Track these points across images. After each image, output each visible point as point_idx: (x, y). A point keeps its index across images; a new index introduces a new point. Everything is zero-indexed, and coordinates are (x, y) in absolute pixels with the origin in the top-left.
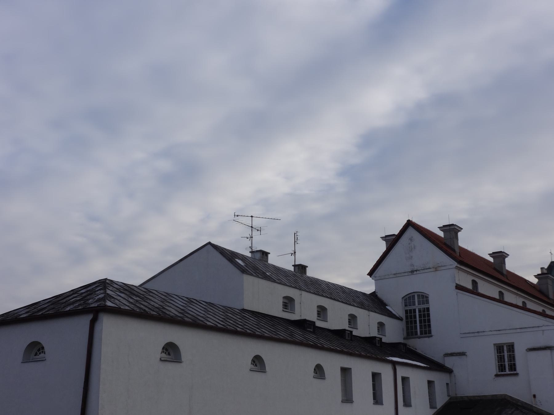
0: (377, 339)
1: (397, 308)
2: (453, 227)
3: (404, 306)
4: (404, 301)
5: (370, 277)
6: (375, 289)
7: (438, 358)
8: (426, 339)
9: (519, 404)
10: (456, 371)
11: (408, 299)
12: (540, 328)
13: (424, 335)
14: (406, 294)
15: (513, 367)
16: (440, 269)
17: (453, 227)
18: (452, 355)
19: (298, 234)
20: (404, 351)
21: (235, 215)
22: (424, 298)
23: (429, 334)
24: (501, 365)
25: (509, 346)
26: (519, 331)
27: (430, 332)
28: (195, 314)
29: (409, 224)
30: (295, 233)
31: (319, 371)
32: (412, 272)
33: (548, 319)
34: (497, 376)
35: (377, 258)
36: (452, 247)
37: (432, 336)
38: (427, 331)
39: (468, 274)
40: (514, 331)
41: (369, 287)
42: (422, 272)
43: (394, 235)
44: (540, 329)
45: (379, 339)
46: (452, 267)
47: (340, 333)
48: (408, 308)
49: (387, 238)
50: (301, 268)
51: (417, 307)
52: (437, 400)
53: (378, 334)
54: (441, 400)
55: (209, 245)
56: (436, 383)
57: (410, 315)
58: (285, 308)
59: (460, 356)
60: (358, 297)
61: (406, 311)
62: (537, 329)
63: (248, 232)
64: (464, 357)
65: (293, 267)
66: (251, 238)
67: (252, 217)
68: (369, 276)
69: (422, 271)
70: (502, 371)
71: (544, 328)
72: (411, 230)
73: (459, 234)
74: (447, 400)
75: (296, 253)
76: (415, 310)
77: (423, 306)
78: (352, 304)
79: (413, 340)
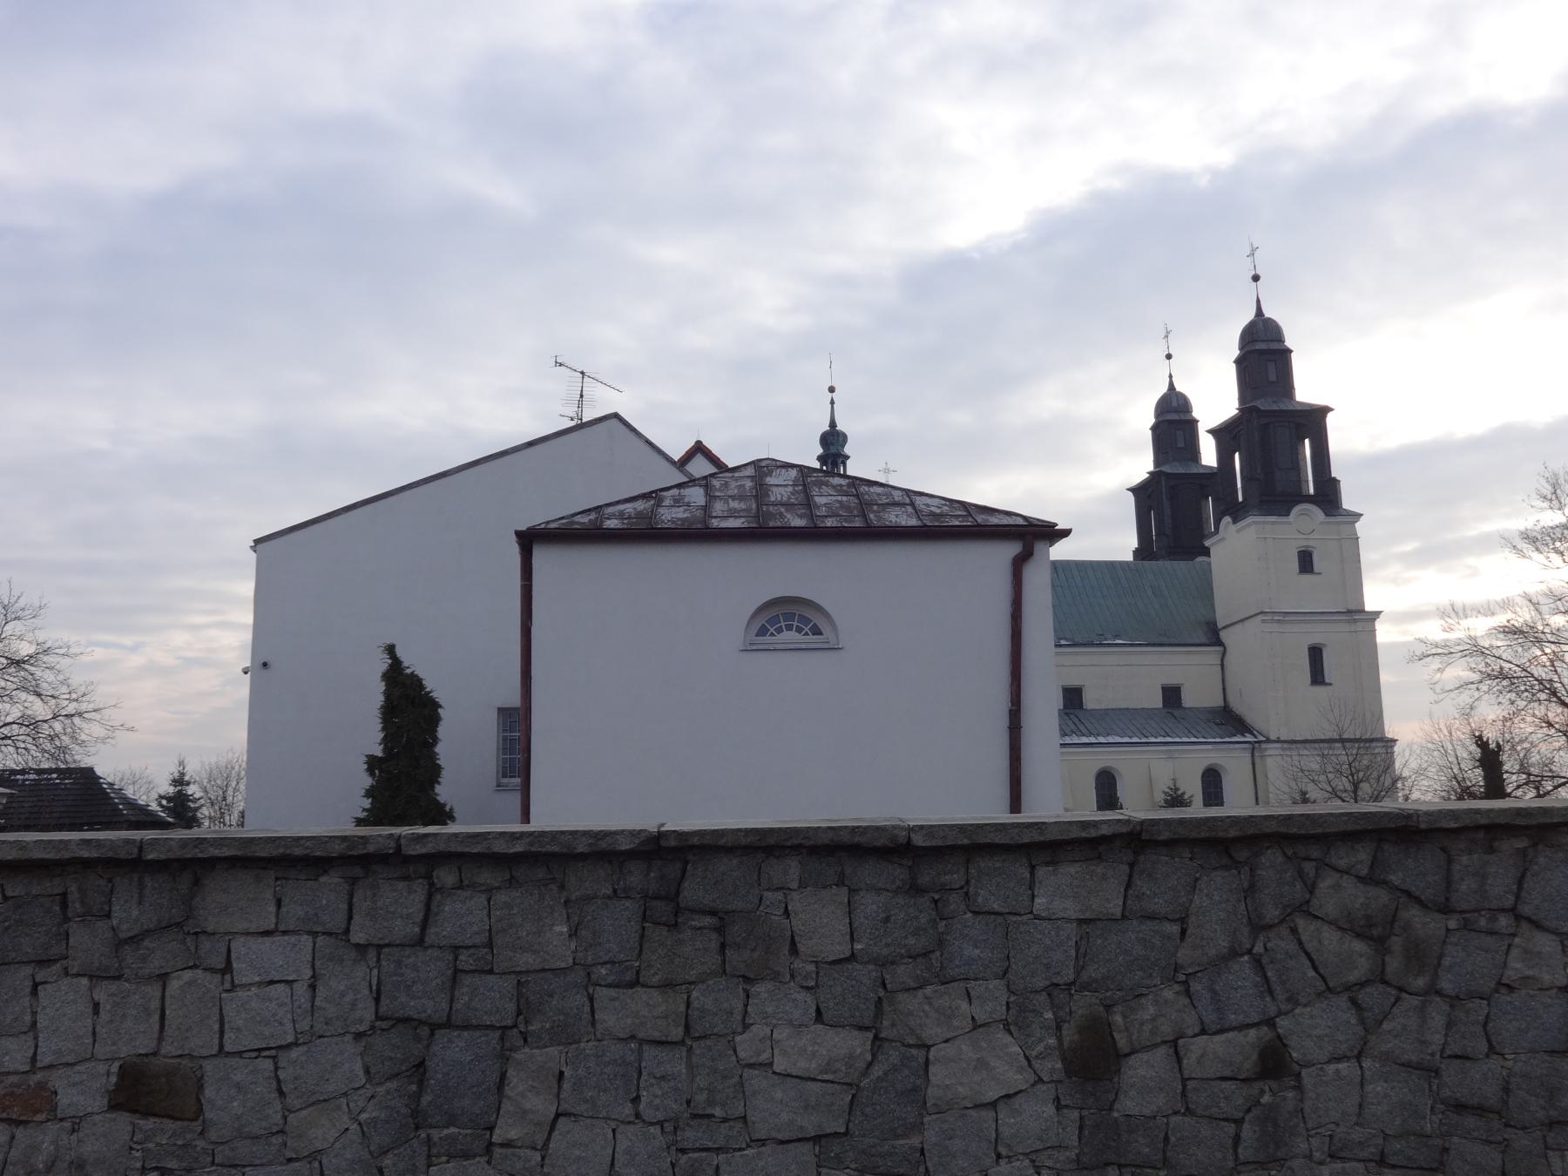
67: (582, 373)
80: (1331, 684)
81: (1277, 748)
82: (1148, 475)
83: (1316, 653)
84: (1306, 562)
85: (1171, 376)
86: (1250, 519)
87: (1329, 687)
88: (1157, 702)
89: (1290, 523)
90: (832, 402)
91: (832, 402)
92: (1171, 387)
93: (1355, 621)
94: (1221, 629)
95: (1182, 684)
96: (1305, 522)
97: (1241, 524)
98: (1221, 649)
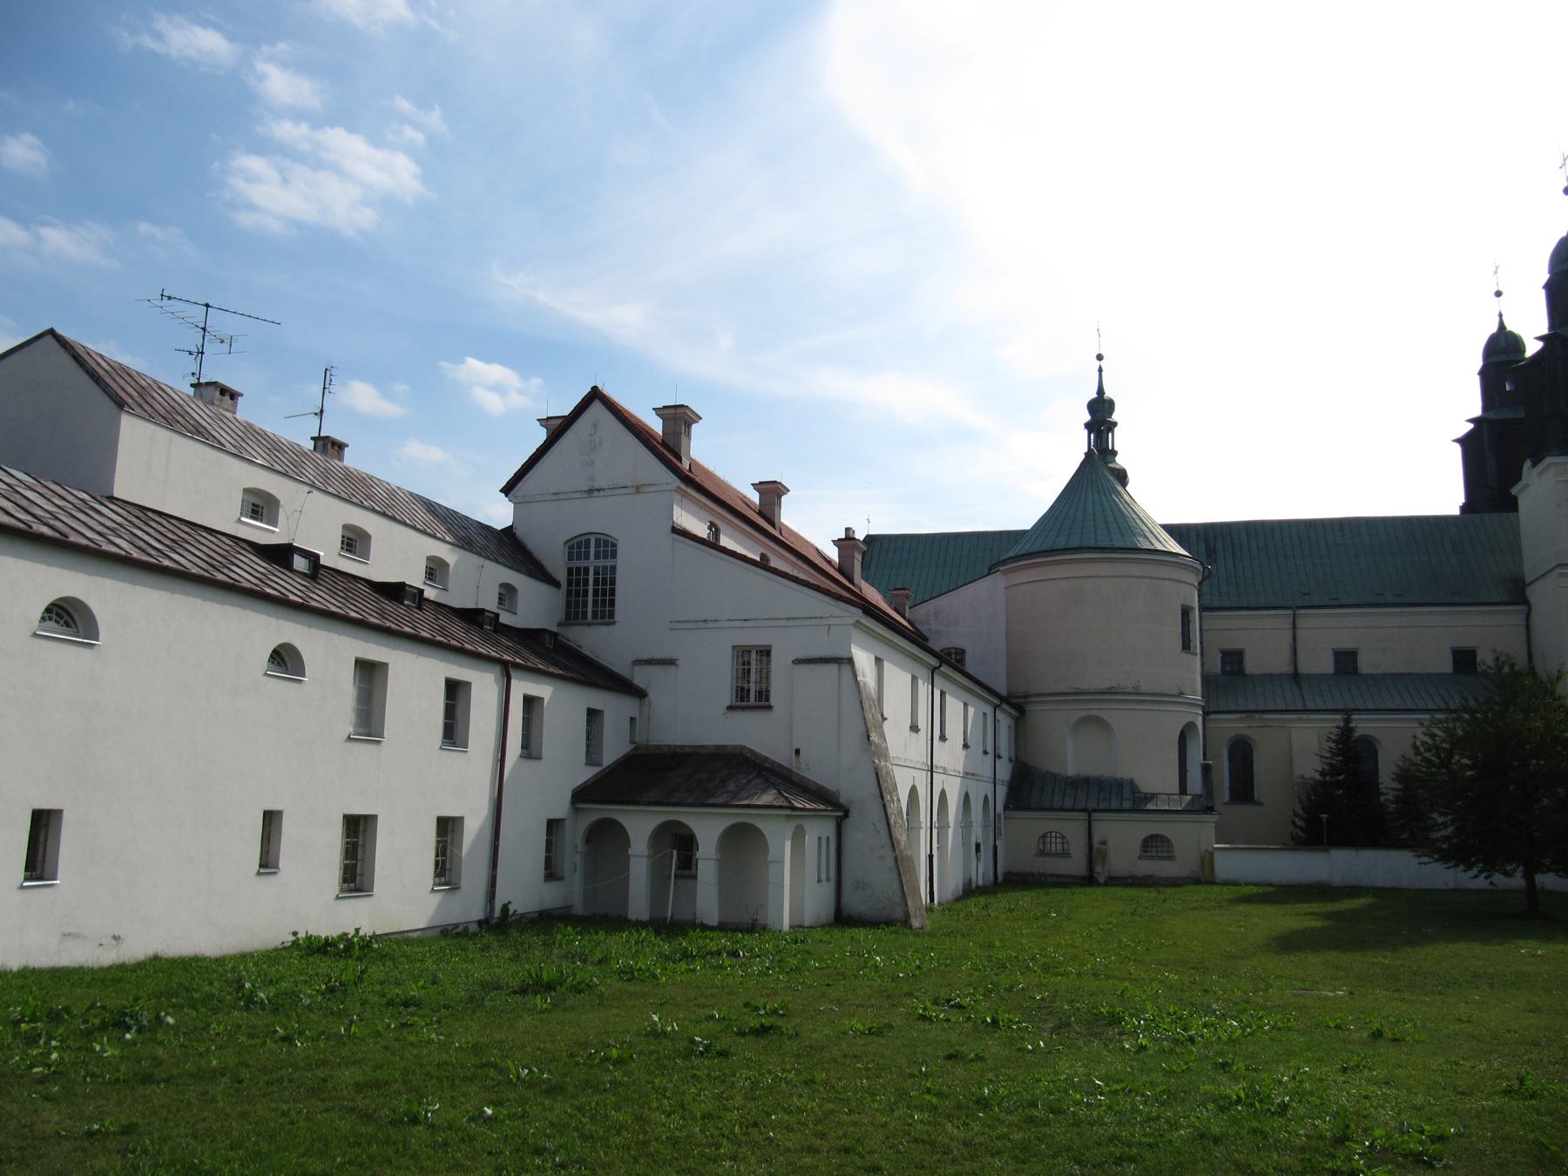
0: (486, 614)
1: (558, 565)
2: (680, 410)
3: (567, 559)
4: (567, 551)
5: (506, 496)
6: (512, 520)
7: (620, 666)
8: (604, 629)
9: (767, 765)
10: (652, 694)
11: (577, 547)
13: (599, 621)
14: (575, 535)
15: (764, 695)
17: (680, 410)
19: (334, 372)
21: (162, 295)
22: (608, 547)
23: (609, 618)
24: (742, 689)
25: (761, 652)
26: (783, 623)
27: (612, 615)
28: (178, 551)
29: (595, 395)
30: (326, 370)
31: (285, 660)
32: (591, 491)
33: (841, 604)
34: (731, 708)
36: (675, 449)
37: (614, 623)
38: (606, 610)
39: (701, 508)
40: (775, 623)
41: (499, 513)
42: (609, 492)
44: (825, 622)
45: (492, 615)
46: (669, 487)
48: (576, 564)
49: (550, 422)
50: (329, 446)
51: (592, 563)
52: (605, 750)
53: (498, 608)
54: (614, 748)
55: (49, 338)
56: (605, 713)
57: (576, 578)
58: (429, 579)
59: (663, 666)
60: (465, 528)
61: (570, 571)
63: (193, 340)
64: (673, 668)
65: (313, 442)
66: (200, 355)
67: (207, 306)
68: (503, 494)
69: (609, 491)
70: (742, 700)
71: (832, 621)
72: (597, 407)
73: (694, 427)
74: (628, 750)
75: (324, 414)
76: (587, 570)
77: (601, 563)
78: (438, 535)
79: (577, 628)
82: (1471, 426)
86: (1548, 460)
88: (1448, 667)
90: (1100, 370)
91: (1100, 370)
92: (1502, 326)
95: (1478, 647)
97: (1541, 466)
98: (1525, 608)
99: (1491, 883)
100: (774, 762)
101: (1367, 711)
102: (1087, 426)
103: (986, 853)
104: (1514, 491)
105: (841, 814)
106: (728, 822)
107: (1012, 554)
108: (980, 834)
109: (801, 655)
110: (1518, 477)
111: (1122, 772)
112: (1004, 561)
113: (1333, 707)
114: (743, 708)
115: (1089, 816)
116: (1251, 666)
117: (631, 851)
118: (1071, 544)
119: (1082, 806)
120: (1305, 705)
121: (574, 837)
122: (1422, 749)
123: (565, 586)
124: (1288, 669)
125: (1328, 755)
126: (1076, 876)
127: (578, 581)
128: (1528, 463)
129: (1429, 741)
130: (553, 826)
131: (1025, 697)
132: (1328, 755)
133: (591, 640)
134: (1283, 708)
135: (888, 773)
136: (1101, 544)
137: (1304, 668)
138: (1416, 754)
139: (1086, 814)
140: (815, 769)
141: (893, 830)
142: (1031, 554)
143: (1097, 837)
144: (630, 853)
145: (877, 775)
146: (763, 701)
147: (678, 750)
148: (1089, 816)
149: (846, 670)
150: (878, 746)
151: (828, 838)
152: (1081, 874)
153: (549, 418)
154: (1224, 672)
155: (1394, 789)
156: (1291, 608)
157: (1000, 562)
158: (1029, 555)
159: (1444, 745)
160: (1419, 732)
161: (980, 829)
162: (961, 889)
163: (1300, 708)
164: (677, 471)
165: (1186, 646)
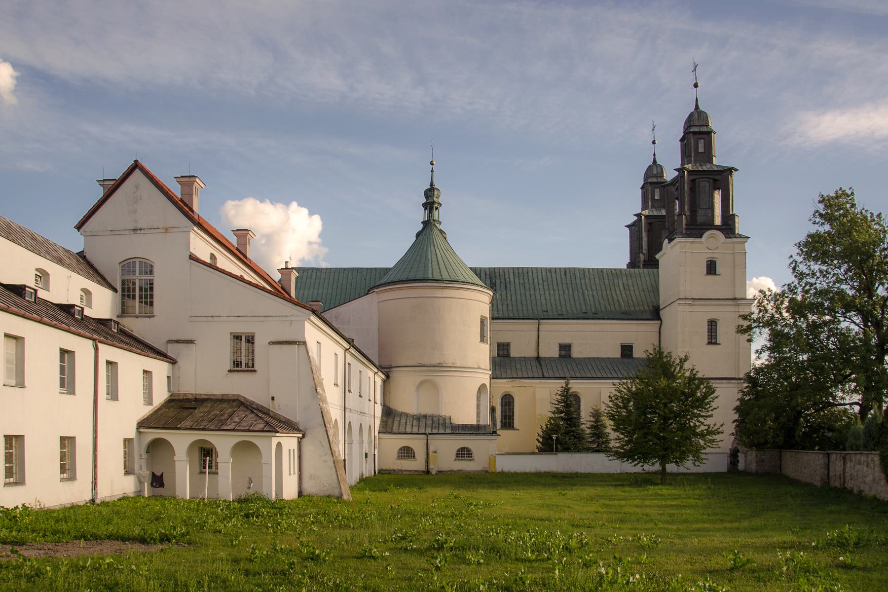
0: (76, 307)
11: (128, 265)
12: (288, 318)
14: (125, 259)
16: (170, 230)
18: (178, 342)
20: (116, 331)
26: (262, 319)
29: (136, 166)
32: (135, 230)
34: (230, 371)
35: (90, 207)
40: (257, 319)
42: (147, 231)
43: (115, 180)
44: (288, 318)
45: (80, 309)
47: (67, 309)
59: (187, 344)
61: (123, 282)
62: (284, 319)
72: (137, 172)
80: (720, 344)
81: (734, 383)
83: (712, 325)
84: (711, 267)
85: (654, 155)
87: (719, 346)
89: (702, 243)
93: (739, 305)
94: (96, 349)
96: (712, 241)
97: (673, 243)
98: (659, 322)
99: (643, 469)
100: (258, 404)
101: (576, 378)
102: (424, 205)
103: (370, 457)
104: (657, 257)
105: (301, 435)
106: (236, 440)
107: (382, 281)
108: (367, 448)
109: (273, 340)
110: (659, 248)
111: (445, 413)
112: (378, 286)
113: (558, 376)
114: (238, 371)
115: (427, 437)
116: (514, 353)
117: (175, 458)
118: (418, 277)
119: (422, 431)
120: (543, 375)
121: (139, 450)
122: (613, 399)
123: (121, 291)
124: (534, 355)
125: (556, 403)
126: (420, 471)
127: (128, 288)
128: (666, 241)
129: (619, 394)
130: (128, 442)
131: (390, 368)
132: (556, 403)
133: (135, 326)
134: (532, 376)
135: (327, 412)
136: (436, 278)
137: (542, 355)
138: (610, 401)
139: (426, 436)
140: (282, 408)
141: (332, 445)
142: (394, 282)
143: (431, 449)
144: (175, 459)
145: (322, 412)
146: (251, 369)
147: (198, 397)
148: (427, 437)
149: (302, 347)
150: (321, 395)
151: (294, 450)
152: (422, 470)
153: (104, 180)
154: (498, 355)
155: (590, 421)
156: (537, 319)
157: (375, 287)
158: (394, 283)
159: (626, 396)
160: (613, 390)
161: (367, 444)
162: (358, 478)
163: (541, 376)
164: (191, 219)
165: (483, 339)
